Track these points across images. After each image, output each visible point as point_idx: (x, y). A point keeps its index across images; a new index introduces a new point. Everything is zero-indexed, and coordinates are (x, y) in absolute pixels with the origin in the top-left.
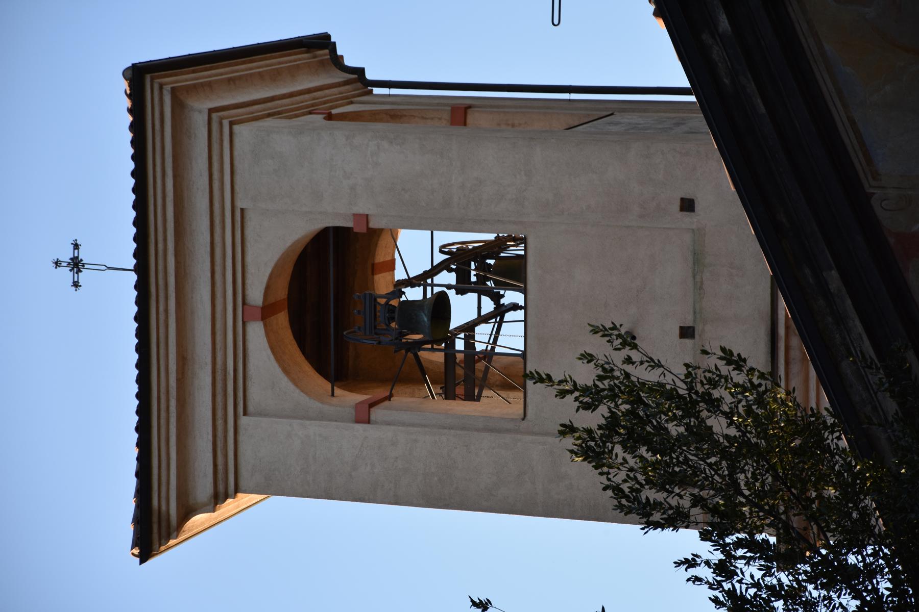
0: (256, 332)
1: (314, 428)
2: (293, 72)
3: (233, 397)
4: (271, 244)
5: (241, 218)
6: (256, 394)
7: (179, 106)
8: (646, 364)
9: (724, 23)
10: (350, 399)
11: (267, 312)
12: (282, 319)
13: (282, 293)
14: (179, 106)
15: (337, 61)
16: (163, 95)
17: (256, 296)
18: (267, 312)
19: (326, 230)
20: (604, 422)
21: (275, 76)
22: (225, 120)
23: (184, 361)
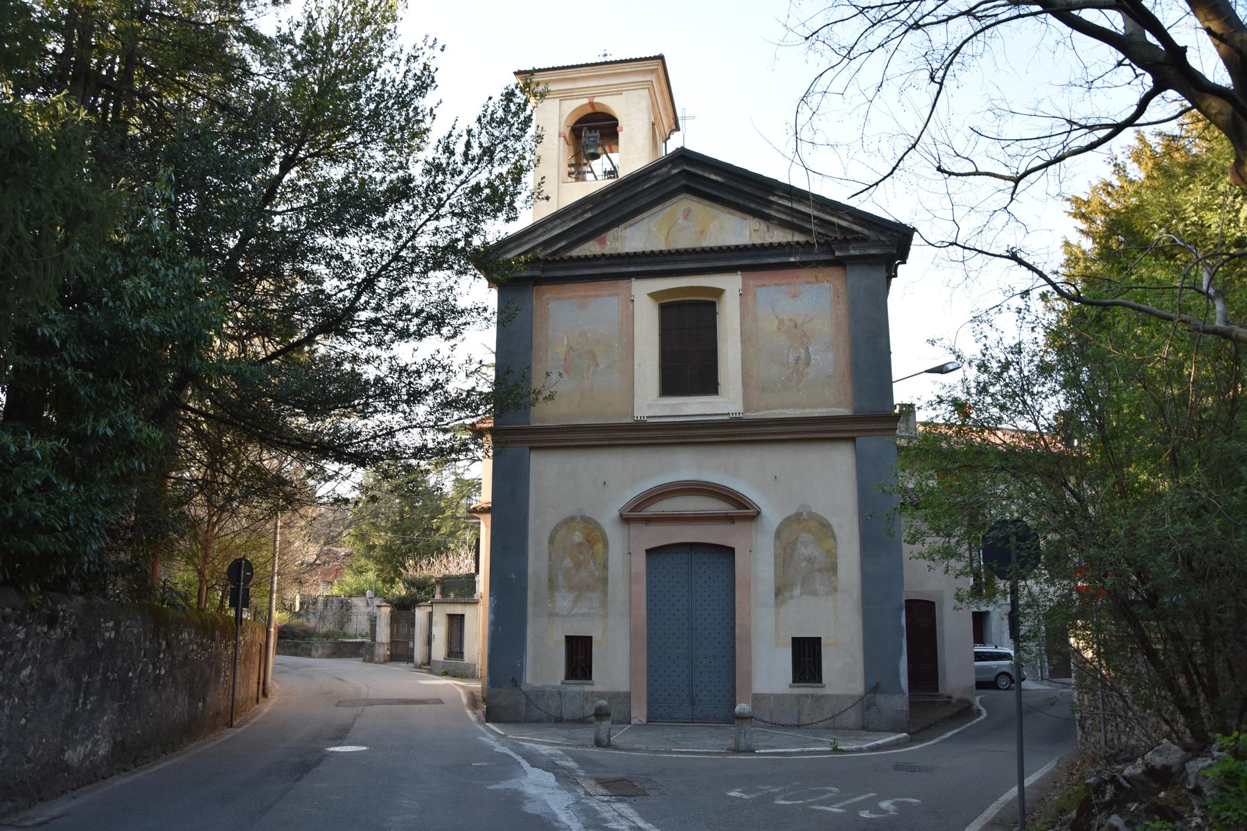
0: (586, 101)
1: (557, 120)
2: (667, 116)
3: (565, 96)
4: (614, 104)
5: (619, 93)
6: (566, 103)
7: (653, 71)
8: (333, 14)
9: (675, 171)
10: (567, 132)
11: (591, 104)
12: (590, 110)
13: (598, 110)
14: (653, 71)
15: (672, 131)
16: (656, 65)
17: (596, 100)
18: (591, 104)
19: (616, 120)
20: (390, 72)
21: (665, 109)
22: (650, 86)
23: (575, 79)
